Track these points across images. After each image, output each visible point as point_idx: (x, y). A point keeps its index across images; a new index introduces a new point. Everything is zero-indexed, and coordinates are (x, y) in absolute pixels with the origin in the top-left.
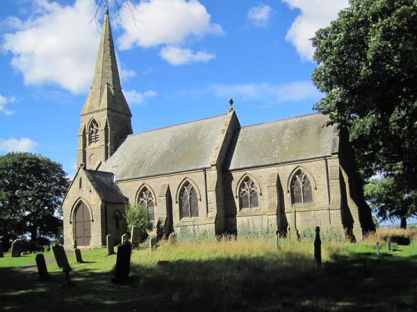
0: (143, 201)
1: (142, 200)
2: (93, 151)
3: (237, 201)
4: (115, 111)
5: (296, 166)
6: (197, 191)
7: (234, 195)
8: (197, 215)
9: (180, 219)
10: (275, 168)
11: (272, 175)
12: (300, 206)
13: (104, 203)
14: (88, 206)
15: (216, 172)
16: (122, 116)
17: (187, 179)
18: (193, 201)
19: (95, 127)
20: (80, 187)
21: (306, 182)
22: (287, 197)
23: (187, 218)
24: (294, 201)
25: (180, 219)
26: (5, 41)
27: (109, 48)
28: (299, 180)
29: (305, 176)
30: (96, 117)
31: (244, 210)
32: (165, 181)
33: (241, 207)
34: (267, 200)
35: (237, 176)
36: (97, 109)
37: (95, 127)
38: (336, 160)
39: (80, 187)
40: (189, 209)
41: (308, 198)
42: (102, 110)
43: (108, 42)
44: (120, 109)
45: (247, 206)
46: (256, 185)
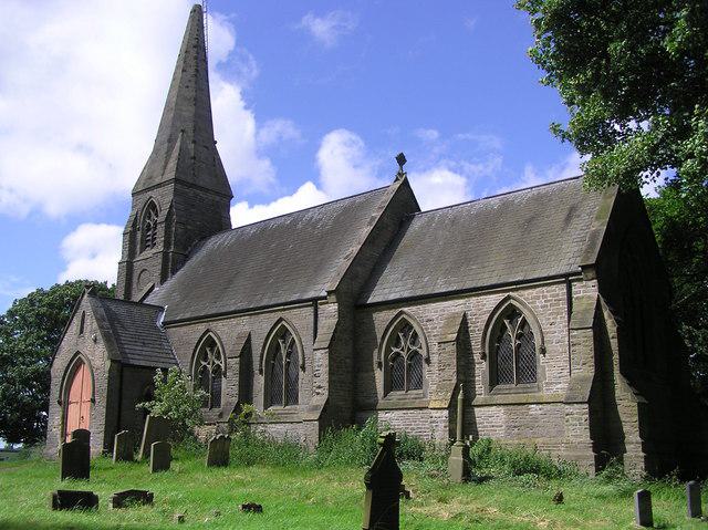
0: (398, 354)
1: (395, 350)
2: (144, 265)
3: (379, 376)
4: (193, 186)
5: (501, 297)
6: (535, 330)
7: (375, 359)
8: (296, 402)
9: (266, 408)
10: (461, 301)
11: (454, 316)
12: (510, 391)
13: (115, 365)
14: (300, 354)
15: (336, 306)
16: (211, 197)
17: (283, 322)
18: (526, 351)
19: (153, 216)
20: (81, 332)
21: (525, 335)
22: (481, 369)
23: (279, 407)
24: (495, 379)
25: (266, 408)
26: (246, 108)
27: (193, 63)
28: (511, 333)
29: (524, 322)
30: (155, 195)
31: (395, 395)
32: (243, 325)
33: (388, 388)
34: (438, 378)
35: (382, 319)
36: (157, 181)
37: (153, 216)
38: (591, 283)
39: (81, 332)
40: (283, 391)
41: (527, 371)
42: (169, 182)
43: (193, 52)
44: (204, 180)
45: (400, 387)
46: (421, 340)
